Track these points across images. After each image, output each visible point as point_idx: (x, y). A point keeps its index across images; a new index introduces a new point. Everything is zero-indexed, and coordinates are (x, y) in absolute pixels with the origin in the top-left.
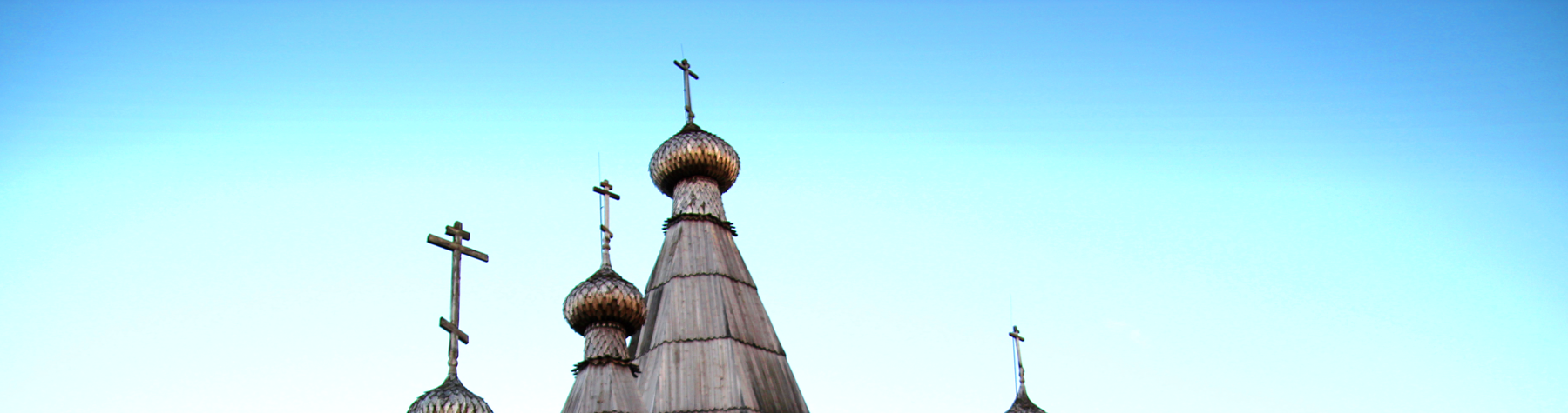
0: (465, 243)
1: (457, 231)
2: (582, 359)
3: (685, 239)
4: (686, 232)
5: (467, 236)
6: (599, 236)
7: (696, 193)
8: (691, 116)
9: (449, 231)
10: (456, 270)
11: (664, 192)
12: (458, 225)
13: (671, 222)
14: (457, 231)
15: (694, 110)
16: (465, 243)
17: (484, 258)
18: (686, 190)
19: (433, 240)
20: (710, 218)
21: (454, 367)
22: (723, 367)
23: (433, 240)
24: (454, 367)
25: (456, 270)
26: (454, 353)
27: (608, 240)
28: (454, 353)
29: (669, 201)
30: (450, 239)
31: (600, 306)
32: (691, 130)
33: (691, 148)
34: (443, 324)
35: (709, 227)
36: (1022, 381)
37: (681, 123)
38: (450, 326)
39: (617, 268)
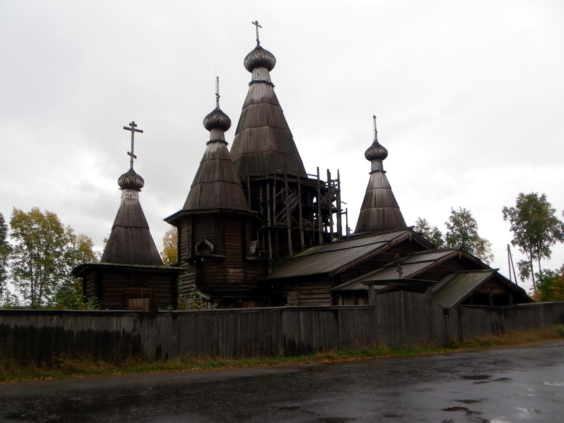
0: (135, 128)
1: (133, 124)
2: (209, 140)
3: (255, 90)
4: (255, 88)
5: (136, 126)
6: (215, 97)
7: (260, 73)
8: (258, 42)
9: (130, 125)
10: (133, 136)
11: (36, 215)
12: (133, 122)
13: (251, 84)
14: (133, 124)
15: (260, 40)
16: (135, 128)
17: (142, 132)
18: (257, 71)
19: (125, 128)
20: (264, 82)
21: (132, 166)
22: (266, 136)
23: (125, 128)
24: (132, 166)
25: (133, 136)
26: (132, 162)
27: (218, 98)
28: (132, 162)
29: (251, 74)
30: (131, 127)
31: (214, 123)
33: (257, 56)
34: (129, 153)
35: (264, 85)
36: (376, 136)
37: (255, 45)
38: (131, 154)
39: (221, 108)
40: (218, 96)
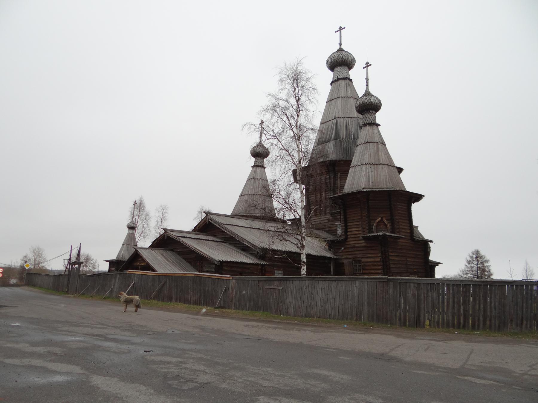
32: (341, 50)
40: (367, 79)
